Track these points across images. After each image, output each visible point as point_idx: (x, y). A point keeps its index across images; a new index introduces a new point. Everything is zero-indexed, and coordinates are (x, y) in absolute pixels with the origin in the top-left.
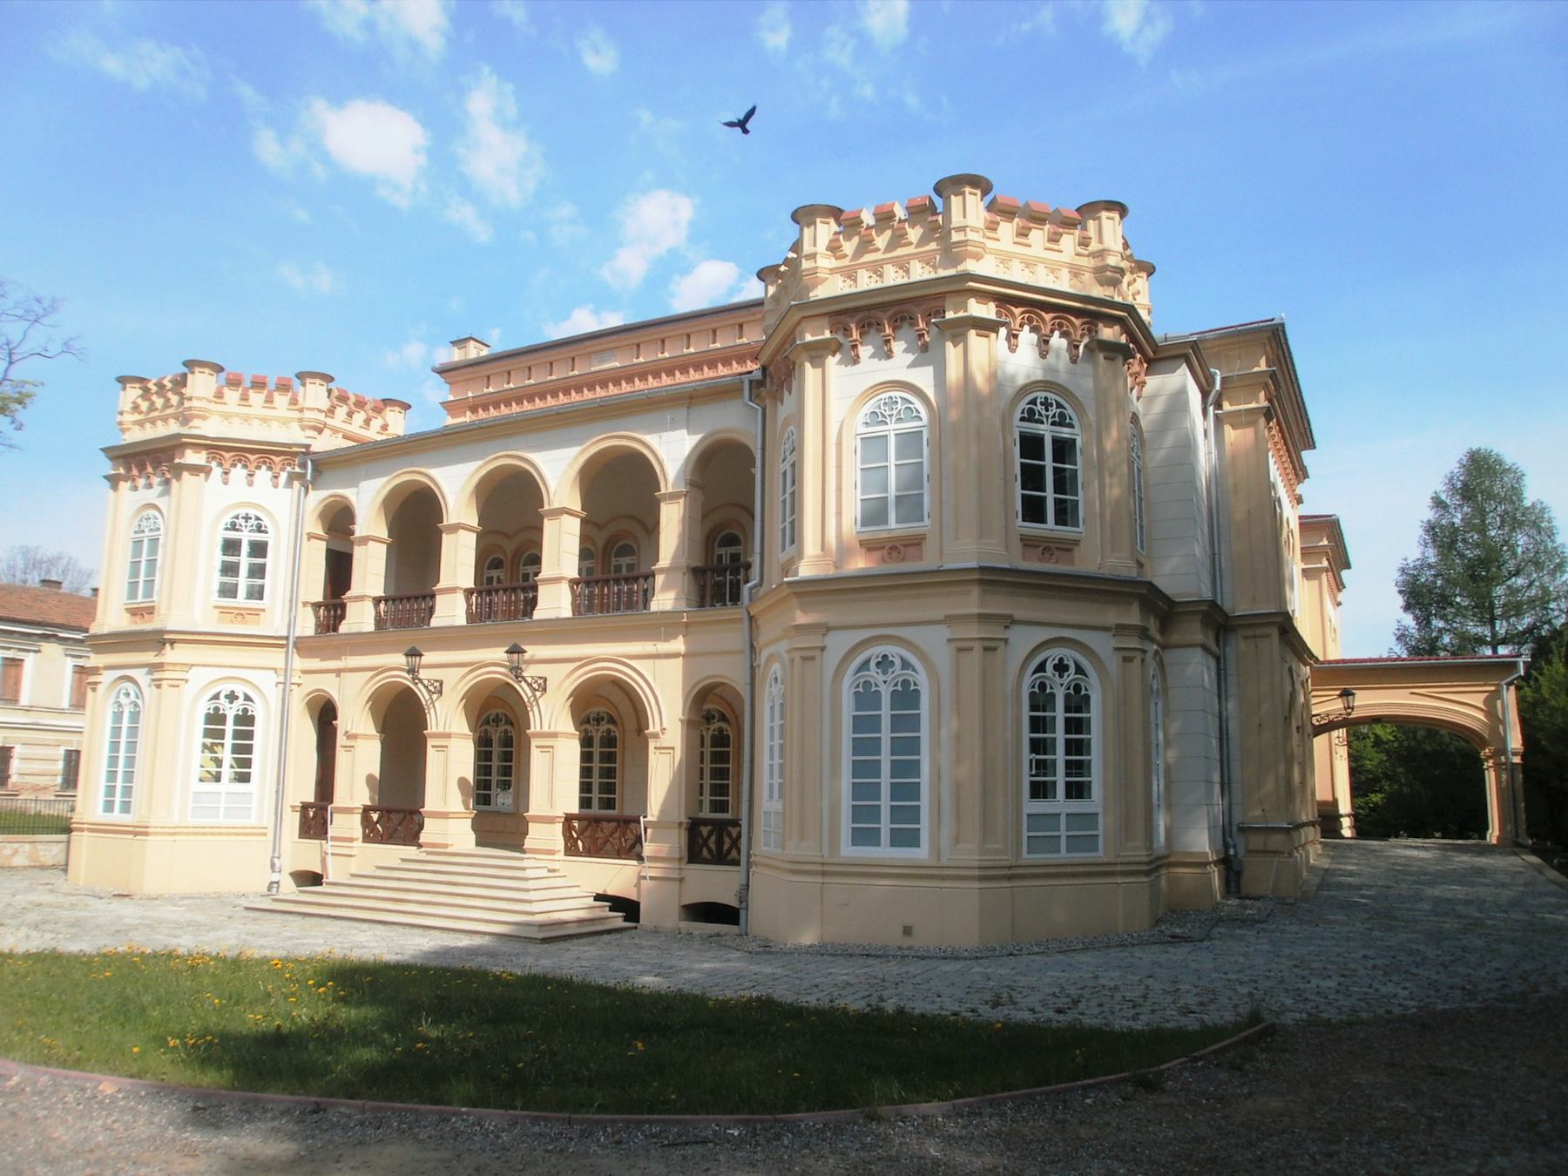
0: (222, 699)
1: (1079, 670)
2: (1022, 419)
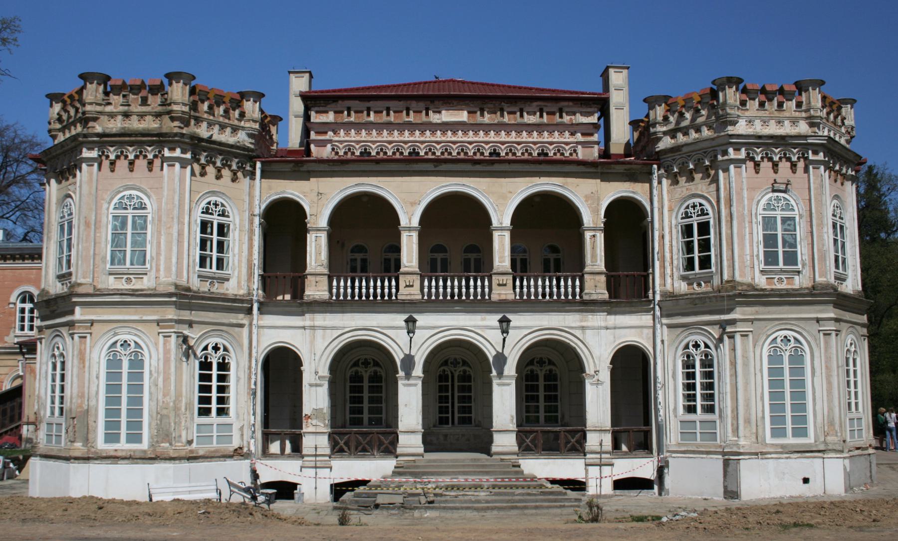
0: (119, 348)
1: (225, 349)
2: (203, 213)
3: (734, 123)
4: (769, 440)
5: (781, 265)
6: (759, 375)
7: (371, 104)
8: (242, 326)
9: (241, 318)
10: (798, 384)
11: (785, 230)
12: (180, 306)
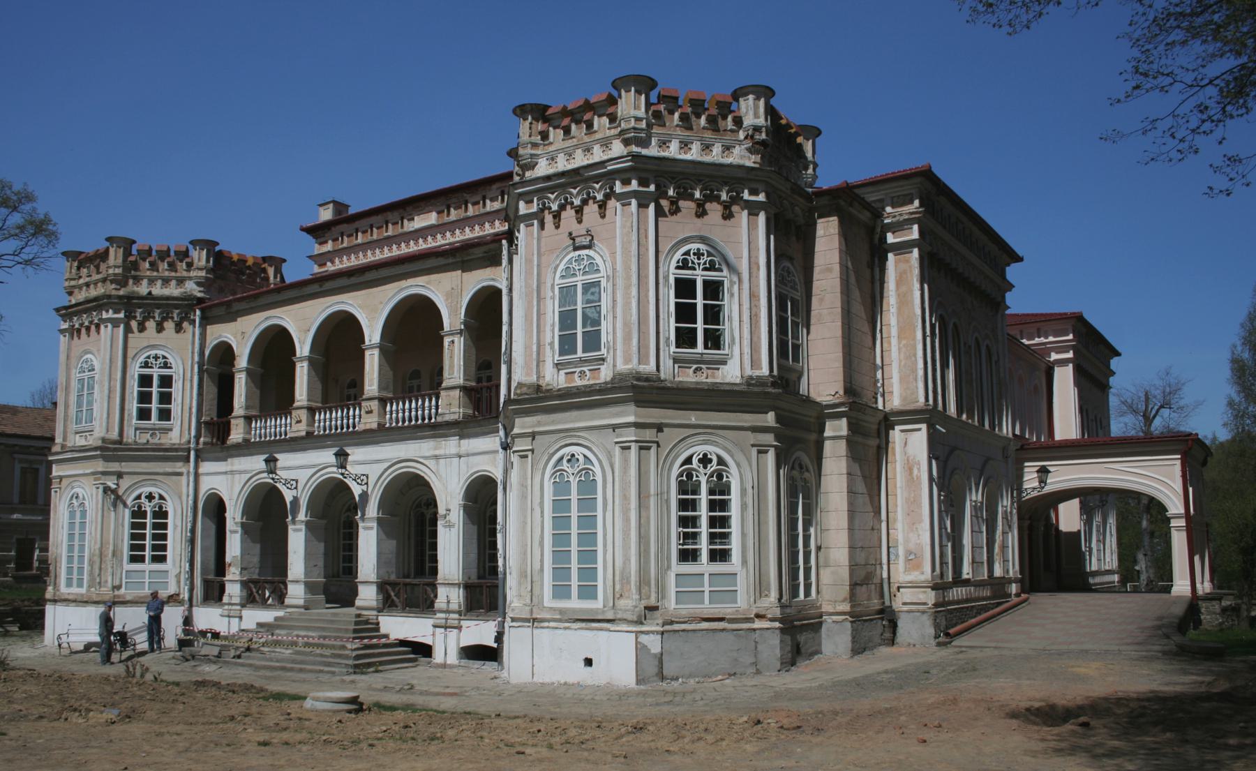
0: (143, 499)
1: (721, 461)
2: (678, 268)
3: (532, 166)
4: (548, 601)
5: (580, 353)
6: (538, 510)
7: (357, 224)
8: (180, 474)
9: (179, 467)
10: (588, 521)
11: (588, 302)
12: (107, 459)
